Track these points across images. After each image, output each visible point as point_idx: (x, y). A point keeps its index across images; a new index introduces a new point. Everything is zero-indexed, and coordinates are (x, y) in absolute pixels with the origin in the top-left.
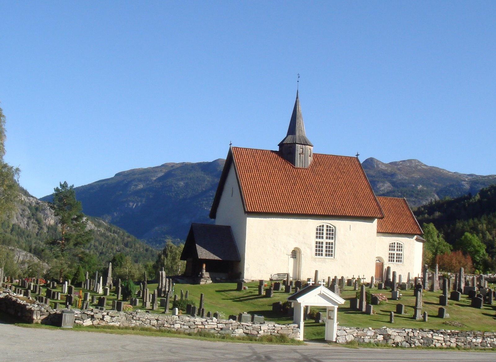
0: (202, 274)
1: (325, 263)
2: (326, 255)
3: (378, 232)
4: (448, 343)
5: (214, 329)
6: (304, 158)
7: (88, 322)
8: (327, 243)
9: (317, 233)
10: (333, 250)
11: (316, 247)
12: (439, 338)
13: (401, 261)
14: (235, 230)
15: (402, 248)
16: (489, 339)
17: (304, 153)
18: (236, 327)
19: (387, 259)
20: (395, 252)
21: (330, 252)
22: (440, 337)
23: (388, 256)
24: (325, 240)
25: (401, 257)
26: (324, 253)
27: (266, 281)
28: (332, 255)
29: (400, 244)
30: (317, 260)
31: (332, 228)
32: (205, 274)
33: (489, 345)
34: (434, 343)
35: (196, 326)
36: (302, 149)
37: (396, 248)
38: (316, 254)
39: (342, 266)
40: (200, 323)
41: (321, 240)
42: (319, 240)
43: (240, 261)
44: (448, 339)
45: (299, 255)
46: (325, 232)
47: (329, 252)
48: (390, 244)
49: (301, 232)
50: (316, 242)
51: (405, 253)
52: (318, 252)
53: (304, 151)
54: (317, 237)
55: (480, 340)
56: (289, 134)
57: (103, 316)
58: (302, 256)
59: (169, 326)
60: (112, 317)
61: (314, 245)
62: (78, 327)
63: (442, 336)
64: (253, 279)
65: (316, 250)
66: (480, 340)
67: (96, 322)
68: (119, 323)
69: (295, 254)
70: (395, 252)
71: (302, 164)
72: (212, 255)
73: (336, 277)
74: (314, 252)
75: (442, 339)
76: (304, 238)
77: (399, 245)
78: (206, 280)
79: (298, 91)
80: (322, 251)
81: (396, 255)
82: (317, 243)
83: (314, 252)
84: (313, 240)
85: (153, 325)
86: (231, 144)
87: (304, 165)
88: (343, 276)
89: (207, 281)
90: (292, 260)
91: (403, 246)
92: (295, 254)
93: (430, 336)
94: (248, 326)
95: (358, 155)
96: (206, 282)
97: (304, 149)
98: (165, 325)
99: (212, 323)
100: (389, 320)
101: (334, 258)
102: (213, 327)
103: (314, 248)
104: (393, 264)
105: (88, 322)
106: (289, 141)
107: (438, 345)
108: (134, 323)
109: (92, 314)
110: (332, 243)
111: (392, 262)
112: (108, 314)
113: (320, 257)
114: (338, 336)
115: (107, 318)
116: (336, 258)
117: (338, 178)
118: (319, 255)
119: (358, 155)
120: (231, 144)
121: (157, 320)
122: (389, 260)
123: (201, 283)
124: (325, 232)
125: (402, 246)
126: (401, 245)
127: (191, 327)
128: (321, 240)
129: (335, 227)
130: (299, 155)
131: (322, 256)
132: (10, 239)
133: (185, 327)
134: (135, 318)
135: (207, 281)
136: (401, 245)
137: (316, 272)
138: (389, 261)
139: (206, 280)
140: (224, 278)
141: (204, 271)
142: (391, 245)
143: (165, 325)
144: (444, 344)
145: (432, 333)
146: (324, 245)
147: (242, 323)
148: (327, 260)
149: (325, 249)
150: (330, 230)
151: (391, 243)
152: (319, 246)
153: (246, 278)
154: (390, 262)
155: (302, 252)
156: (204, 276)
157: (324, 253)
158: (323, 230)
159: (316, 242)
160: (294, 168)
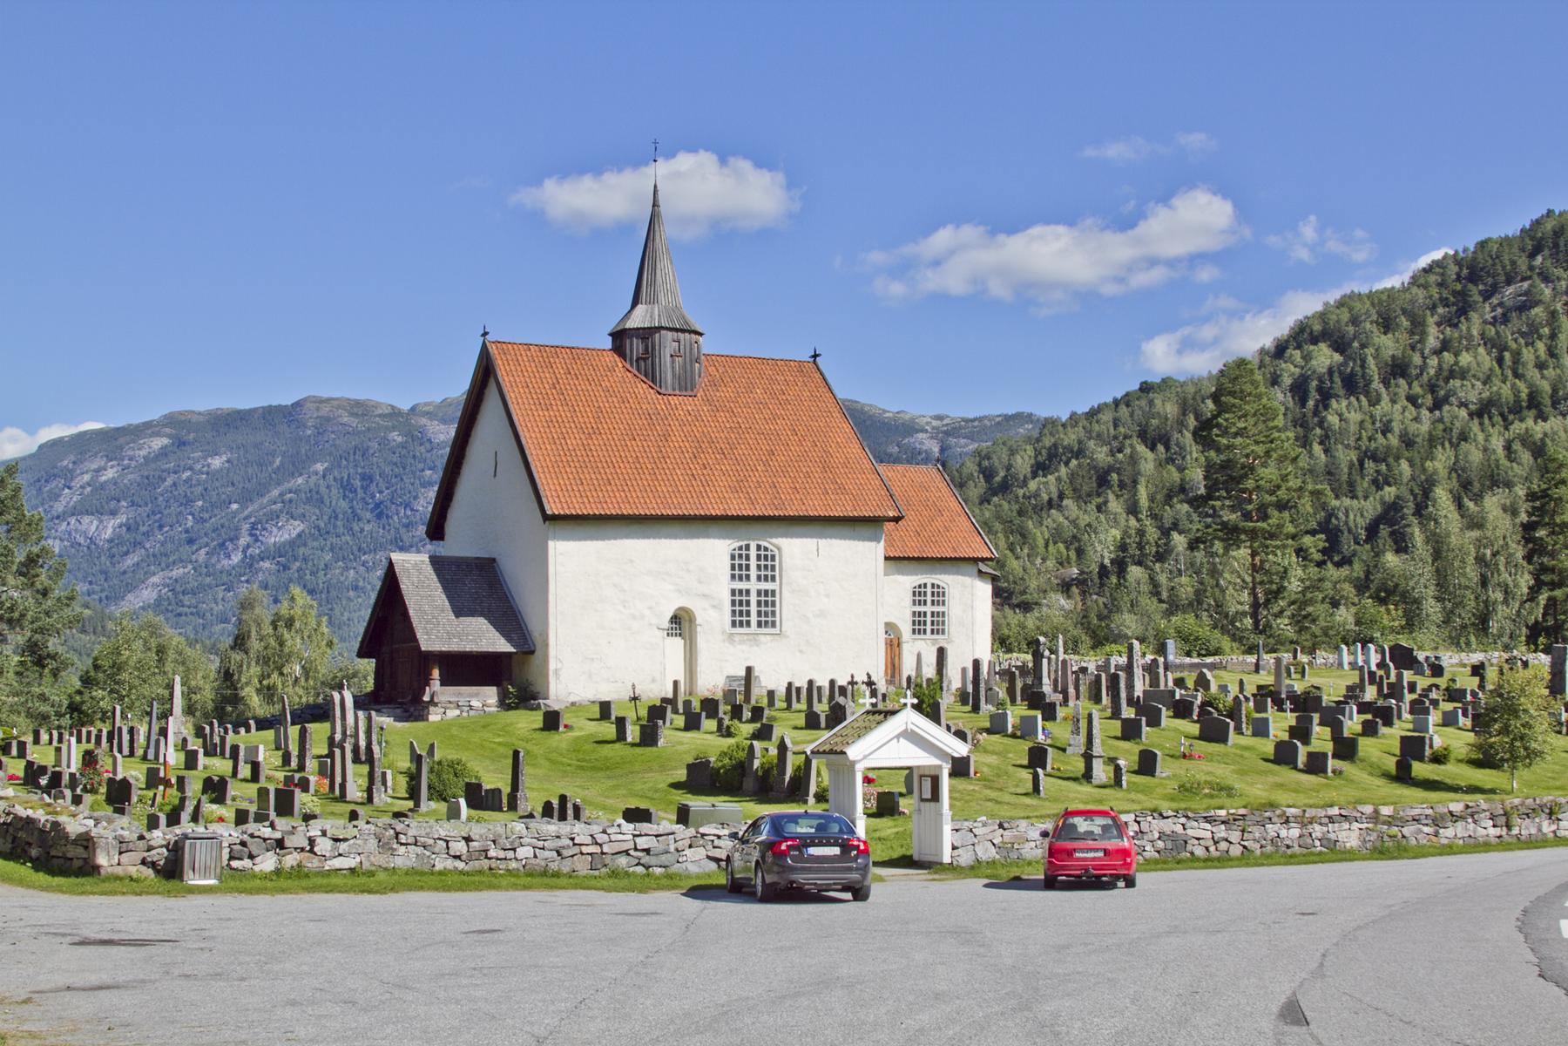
2: (759, 624)
3: (887, 558)
4: (1223, 846)
5: (626, 852)
7: (267, 862)
8: (759, 593)
9: (733, 567)
11: (733, 603)
12: (1201, 834)
16: (1317, 827)
18: (687, 842)
20: (929, 609)
21: (768, 620)
22: (1202, 830)
23: (909, 618)
24: (753, 585)
26: (754, 619)
27: (619, 702)
28: (774, 624)
30: (737, 638)
33: (1317, 843)
34: (1189, 847)
35: (576, 850)
37: (929, 598)
38: (734, 624)
40: (589, 840)
41: (764, 586)
42: (739, 585)
43: (532, 652)
44: (1223, 834)
46: (753, 563)
47: (766, 614)
51: (954, 609)
52: (739, 618)
55: (1295, 832)
57: (312, 841)
58: (699, 629)
59: (502, 854)
60: (336, 840)
61: (727, 598)
62: (235, 880)
63: (1208, 826)
64: (572, 699)
66: (1295, 832)
67: (291, 860)
68: (358, 859)
70: (929, 609)
72: (503, 641)
74: (728, 618)
75: (1209, 835)
81: (930, 619)
82: (733, 592)
83: (728, 618)
84: (723, 587)
85: (455, 857)
86: (485, 334)
92: (681, 622)
93: (1179, 829)
94: (719, 837)
95: (815, 356)
98: (492, 853)
99: (620, 837)
100: (1029, 786)
102: (624, 847)
103: (728, 608)
105: (267, 862)
107: (1199, 852)
108: (405, 858)
109: (278, 835)
112: (324, 833)
113: (744, 630)
114: (954, 848)
115: (324, 845)
119: (815, 356)
120: (485, 334)
121: (468, 839)
123: (432, 718)
124: (753, 563)
127: (565, 853)
128: (764, 586)
129: (779, 549)
130: (668, 359)
132: (1545, 420)
133: (547, 854)
134: (403, 839)
143: (492, 853)
144: (1212, 849)
145: (1183, 820)
146: (753, 599)
147: (702, 830)
148: (762, 638)
149: (755, 610)
150: (766, 557)
152: (739, 601)
157: (754, 619)
158: (748, 558)
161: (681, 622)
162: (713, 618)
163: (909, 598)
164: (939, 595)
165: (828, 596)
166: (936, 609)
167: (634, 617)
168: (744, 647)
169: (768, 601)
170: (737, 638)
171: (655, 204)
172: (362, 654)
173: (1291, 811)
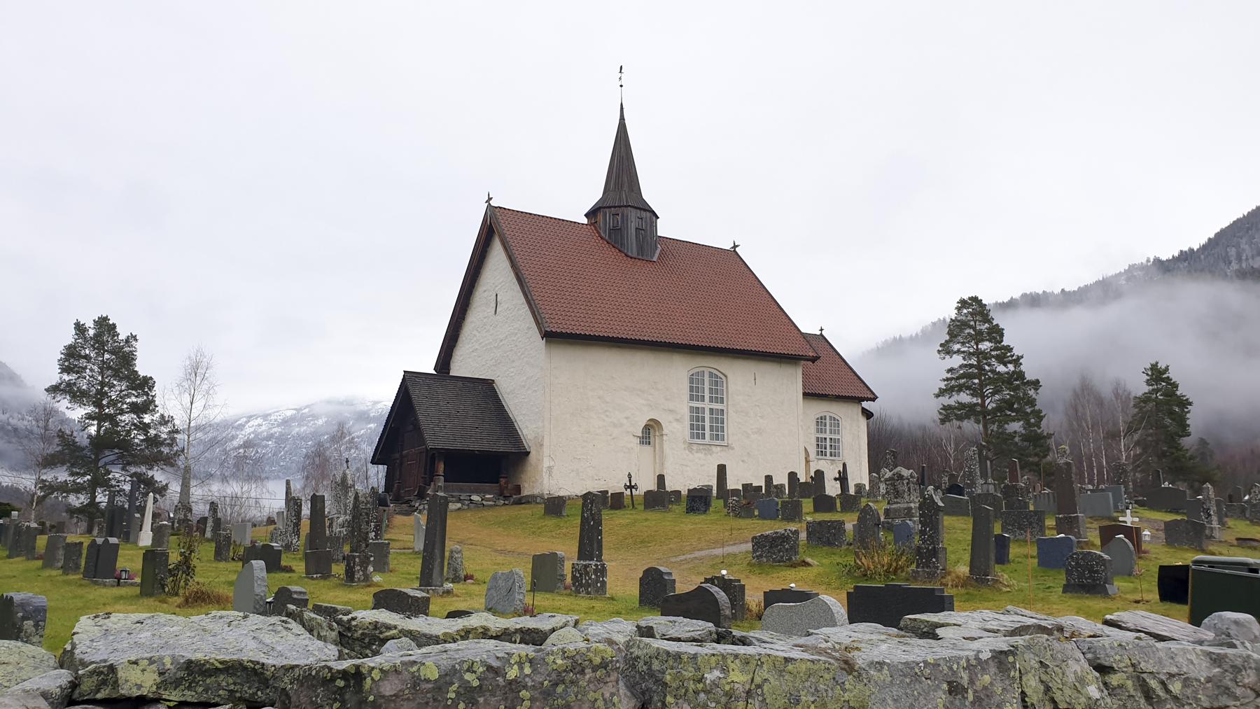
20: (828, 436)
21: (718, 432)
24: (707, 405)
38: (692, 436)
42: (696, 404)
49: (663, 386)
52: (697, 430)
54: (692, 399)
73: (769, 479)
74: (687, 431)
103: (687, 423)
120: (490, 199)
130: (633, 231)
137: (722, 470)
148: (714, 448)
149: (707, 427)
161: (650, 431)
162: (676, 428)
163: (813, 427)
164: (836, 423)
165: (762, 417)
166: (833, 436)
167: (615, 426)
168: (699, 455)
169: (719, 419)
170: (695, 447)
171: (622, 118)
172: (375, 461)
173: (560, 689)
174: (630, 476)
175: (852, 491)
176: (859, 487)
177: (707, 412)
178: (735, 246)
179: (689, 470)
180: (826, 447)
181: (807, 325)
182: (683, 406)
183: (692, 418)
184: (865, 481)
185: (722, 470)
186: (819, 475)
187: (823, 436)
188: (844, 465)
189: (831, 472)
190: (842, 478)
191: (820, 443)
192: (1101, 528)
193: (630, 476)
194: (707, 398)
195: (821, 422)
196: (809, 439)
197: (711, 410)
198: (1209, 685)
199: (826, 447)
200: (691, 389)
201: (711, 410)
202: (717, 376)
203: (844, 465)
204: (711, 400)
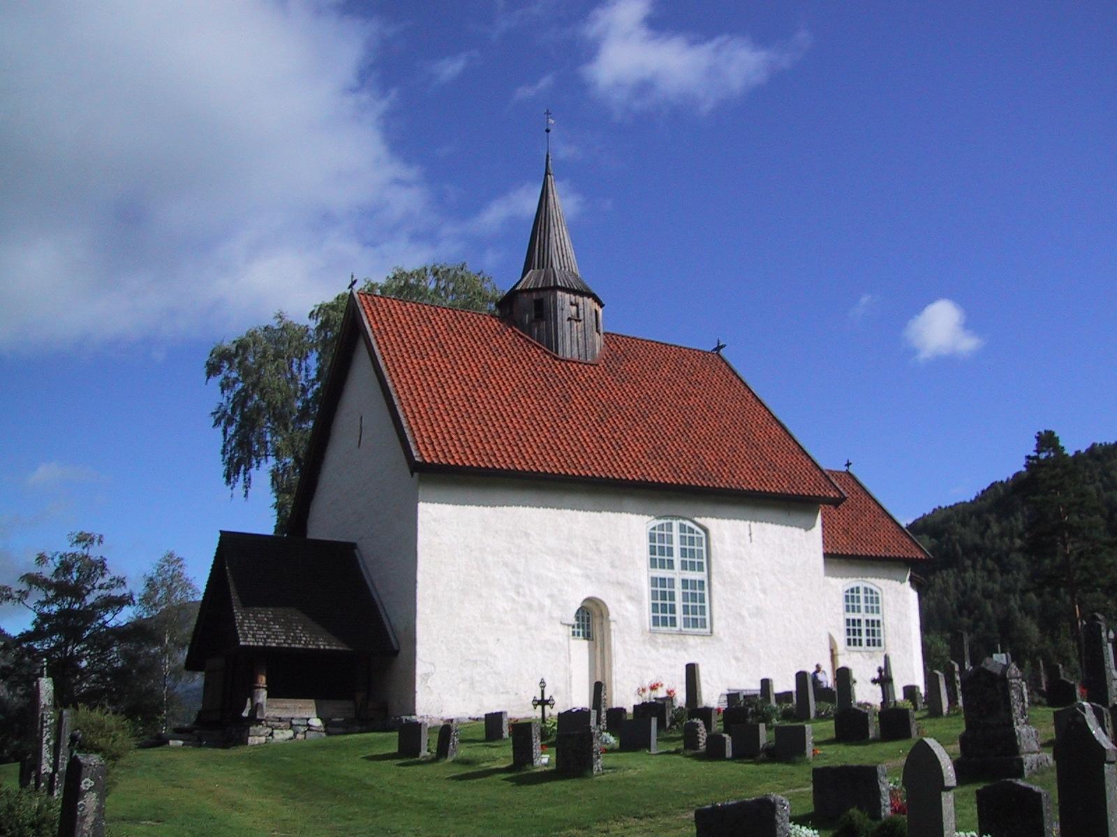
0: (256, 708)
1: (685, 650)
6: (579, 331)
10: (707, 604)
13: (879, 641)
14: (369, 552)
15: (877, 602)
17: (581, 317)
19: (843, 638)
21: (698, 618)
23: (843, 627)
24: (677, 574)
25: (879, 631)
29: (872, 592)
31: (698, 533)
32: (264, 707)
36: (574, 308)
39: (737, 659)
45: (602, 630)
48: (847, 592)
49: (609, 546)
50: (652, 578)
52: (663, 615)
53: (581, 312)
54: (653, 563)
56: (528, 266)
58: (613, 626)
61: (646, 589)
65: (655, 606)
69: (590, 620)
71: (576, 348)
73: (766, 683)
74: (648, 614)
76: (613, 566)
77: (869, 595)
78: (269, 730)
79: (548, 156)
80: (673, 610)
87: (582, 351)
88: (798, 670)
89: (275, 731)
90: (581, 648)
91: (880, 596)
92: (590, 620)
96: (271, 734)
97: (581, 306)
101: (711, 632)
104: (859, 654)
106: (531, 280)
110: (702, 582)
111: (858, 648)
116: (718, 633)
117: (687, 396)
118: (664, 624)
122: (849, 640)
125: (877, 598)
126: (874, 596)
131: (675, 625)
135: (275, 731)
136: (874, 596)
137: (691, 670)
138: (849, 644)
139: (269, 730)
140: (337, 719)
141: (264, 693)
142: (850, 594)
149: (681, 605)
151: (647, 684)
153: (425, 714)
154: (852, 647)
155: (613, 616)
156: (262, 714)
159: (652, 578)
160: (556, 359)
162: (630, 613)
163: (841, 604)
164: (873, 600)
166: (871, 617)
168: (669, 651)
169: (697, 595)
174: (543, 684)
175: (899, 695)
176: (910, 691)
177: (678, 584)
178: (719, 348)
179: (644, 668)
180: (864, 632)
181: (829, 461)
182: (642, 575)
183: (654, 595)
184: (919, 681)
185: (691, 670)
186: (843, 676)
187: (856, 616)
188: (886, 659)
189: (863, 668)
190: (884, 679)
191: (853, 628)
192: (1054, 713)
193: (543, 684)
194: (677, 564)
195: (851, 598)
196: (835, 622)
197: (685, 582)
198: (276, 424)
199: (864, 632)
200: (653, 552)
201: (685, 582)
202: (691, 530)
203: (886, 659)
204: (684, 566)
